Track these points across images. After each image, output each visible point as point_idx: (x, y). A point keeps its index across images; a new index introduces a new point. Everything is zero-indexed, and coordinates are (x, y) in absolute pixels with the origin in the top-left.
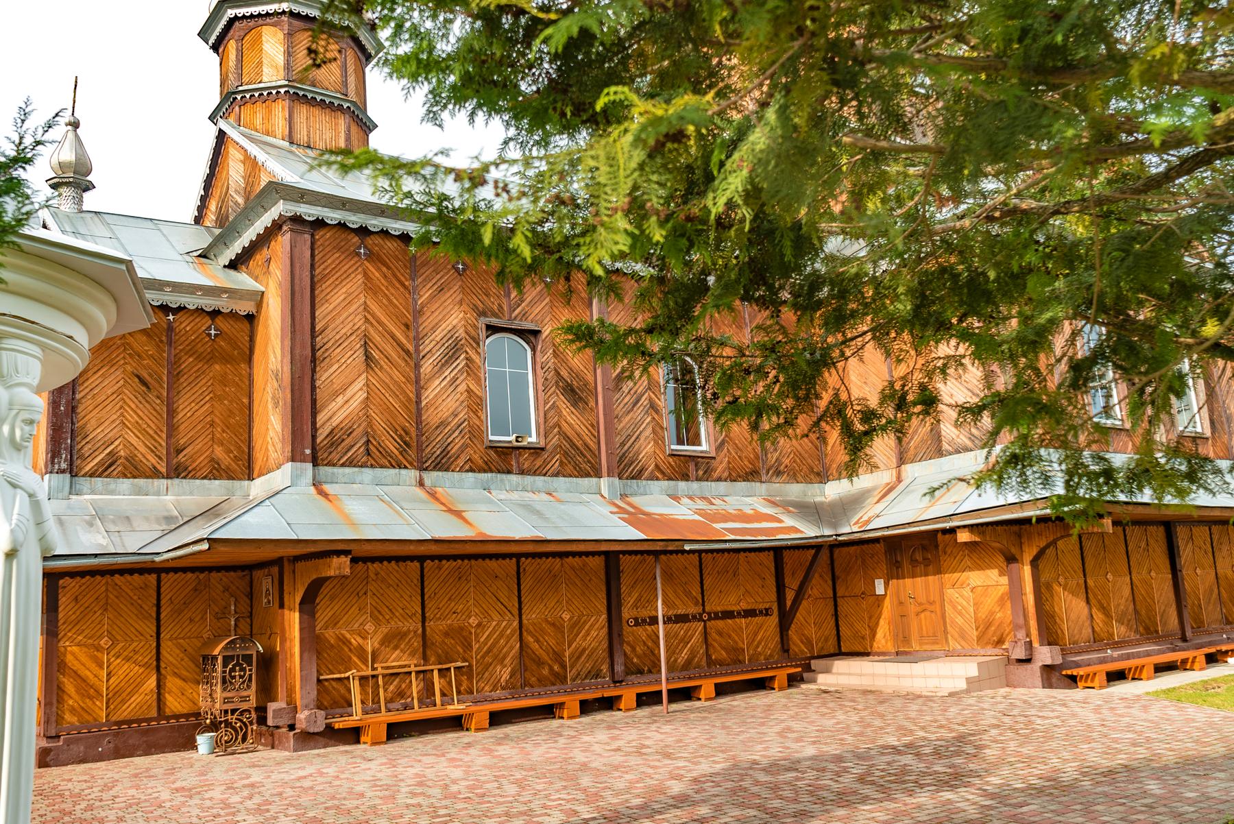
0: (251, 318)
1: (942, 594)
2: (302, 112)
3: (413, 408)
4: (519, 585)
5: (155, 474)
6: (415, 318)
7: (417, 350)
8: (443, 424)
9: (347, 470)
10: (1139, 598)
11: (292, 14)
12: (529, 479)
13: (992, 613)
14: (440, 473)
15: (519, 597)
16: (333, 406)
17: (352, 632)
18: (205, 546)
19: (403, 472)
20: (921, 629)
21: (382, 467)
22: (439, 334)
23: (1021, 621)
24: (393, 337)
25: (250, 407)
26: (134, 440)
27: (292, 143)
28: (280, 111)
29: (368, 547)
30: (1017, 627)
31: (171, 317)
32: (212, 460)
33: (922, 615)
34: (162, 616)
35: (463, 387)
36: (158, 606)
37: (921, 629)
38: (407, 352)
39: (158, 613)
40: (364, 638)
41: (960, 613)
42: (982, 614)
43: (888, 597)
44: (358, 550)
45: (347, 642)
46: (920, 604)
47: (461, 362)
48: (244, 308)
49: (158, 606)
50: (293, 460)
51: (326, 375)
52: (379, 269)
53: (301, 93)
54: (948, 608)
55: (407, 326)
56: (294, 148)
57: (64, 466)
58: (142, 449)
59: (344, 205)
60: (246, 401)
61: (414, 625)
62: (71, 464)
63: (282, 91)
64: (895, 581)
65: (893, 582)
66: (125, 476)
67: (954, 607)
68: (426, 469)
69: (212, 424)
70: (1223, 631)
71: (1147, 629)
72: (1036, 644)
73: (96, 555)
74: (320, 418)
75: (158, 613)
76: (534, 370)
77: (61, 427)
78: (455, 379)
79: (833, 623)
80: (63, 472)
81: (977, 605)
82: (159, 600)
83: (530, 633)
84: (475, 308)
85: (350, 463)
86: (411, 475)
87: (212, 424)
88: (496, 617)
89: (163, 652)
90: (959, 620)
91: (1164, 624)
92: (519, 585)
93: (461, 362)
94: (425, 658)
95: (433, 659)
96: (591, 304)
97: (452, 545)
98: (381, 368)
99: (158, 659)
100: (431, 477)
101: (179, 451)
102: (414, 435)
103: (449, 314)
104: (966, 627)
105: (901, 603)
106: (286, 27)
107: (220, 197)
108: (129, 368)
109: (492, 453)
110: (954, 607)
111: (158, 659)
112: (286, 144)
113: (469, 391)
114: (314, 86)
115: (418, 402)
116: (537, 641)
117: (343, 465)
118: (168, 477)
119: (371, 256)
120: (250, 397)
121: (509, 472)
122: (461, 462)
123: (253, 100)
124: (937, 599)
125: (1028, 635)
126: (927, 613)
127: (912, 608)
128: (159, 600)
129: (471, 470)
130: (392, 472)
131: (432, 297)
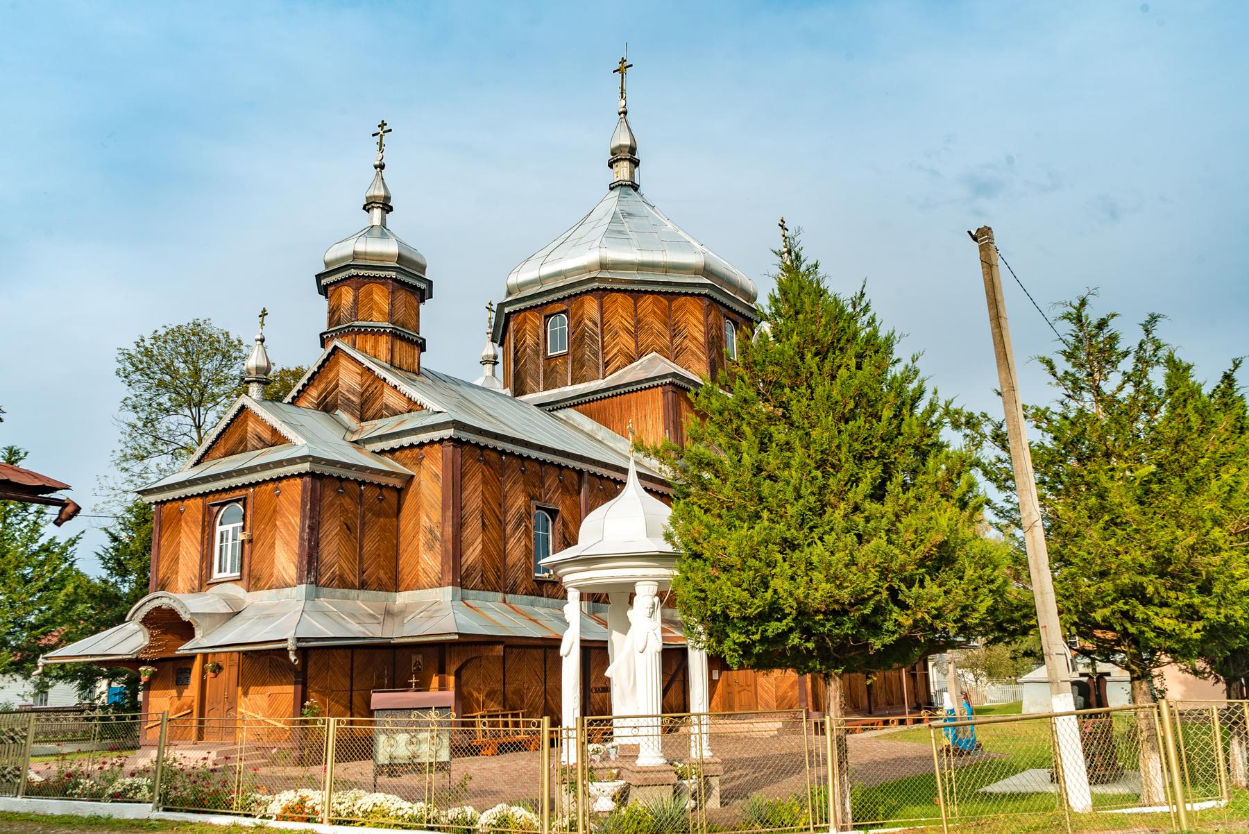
0: (400, 492)
1: (756, 681)
2: (398, 343)
3: (502, 555)
4: (545, 665)
5: (353, 587)
6: (504, 500)
7: (505, 520)
8: (514, 565)
9: (474, 592)
10: (852, 687)
11: (395, 280)
12: (551, 601)
13: (786, 692)
14: (513, 595)
15: (545, 672)
16: (469, 553)
17: (474, 689)
18: (457, 637)
19: (497, 594)
20: (740, 701)
21: (489, 590)
22: (513, 510)
23: (804, 697)
24: (494, 511)
25: (397, 545)
26: (344, 565)
27: (391, 365)
28: (384, 344)
29: (514, 640)
30: (801, 701)
31: (362, 488)
32: (379, 579)
33: (743, 693)
34: (354, 675)
35: (523, 543)
36: (352, 669)
37: (740, 701)
38: (500, 521)
39: (352, 673)
40: (479, 693)
41: (766, 692)
42: (780, 693)
43: (720, 682)
44: (507, 642)
45: (472, 695)
46: (741, 686)
47: (522, 528)
48: (398, 483)
49: (352, 669)
50: (453, 585)
51: (466, 534)
52: (488, 470)
53: (398, 333)
54: (759, 689)
55: (500, 505)
56: (393, 369)
57: (313, 579)
58: (348, 571)
59: (480, 432)
60: (395, 542)
61: (499, 687)
62: (316, 579)
63: (388, 331)
64: (725, 672)
65: (725, 673)
66: (339, 588)
67: (763, 689)
68: (507, 593)
69: (379, 555)
70: (886, 709)
71: (855, 705)
72: (811, 711)
73: (364, 638)
74: (463, 560)
75: (352, 673)
76: (553, 533)
77: (312, 555)
78: (520, 538)
79: (44, 753)
80: (312, 583)
81: (777, 687)
82: (352, 665)
83: (549, 694)
84: (529, 495)
85: (474, 588)
86: (500, 595)
87: (379, 555)
88: (535, 684)
89: (354, 699)
90: (766, 696)
91: (862, 703)
92: (545, 665)
93: (522, 528)
94: (504, 707)
95: (507, 708)
96: (579, 493)
97: (548, 641)
98: (489, 531)
99: (351, 703)
100: (509, 597)
101: (364, 572)
102: (502, 571)
103: (518, 498)
104: (770, 700)
105: (729, 685)
106: (391, 287)
107: (325, 389)
108: (342, 518)
109: (535, 583)
110: (763, 689)
111: (351, 703)
112: (387, 366)
113: (526, 545)
114: (403, 327)
115: (505, 552)
116: (552, 699)
117: (472, 589)
118: (359, 589)
119: (486, 463)
120: (397, 539)
121: (542, 596)
122: (521, 589)
123: (366, 332)
124: (753, 683)
125: (807, 705)
126: (746, 692)
127: (737, 689)
128: (352, 665)
129: (526, 594)
130: (492, 593)
131: (511, 487)
